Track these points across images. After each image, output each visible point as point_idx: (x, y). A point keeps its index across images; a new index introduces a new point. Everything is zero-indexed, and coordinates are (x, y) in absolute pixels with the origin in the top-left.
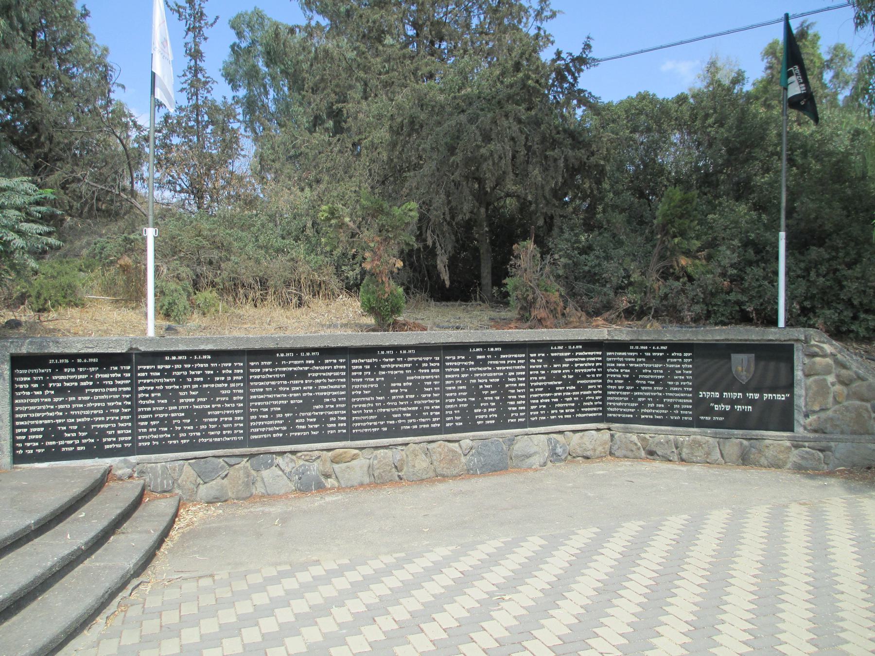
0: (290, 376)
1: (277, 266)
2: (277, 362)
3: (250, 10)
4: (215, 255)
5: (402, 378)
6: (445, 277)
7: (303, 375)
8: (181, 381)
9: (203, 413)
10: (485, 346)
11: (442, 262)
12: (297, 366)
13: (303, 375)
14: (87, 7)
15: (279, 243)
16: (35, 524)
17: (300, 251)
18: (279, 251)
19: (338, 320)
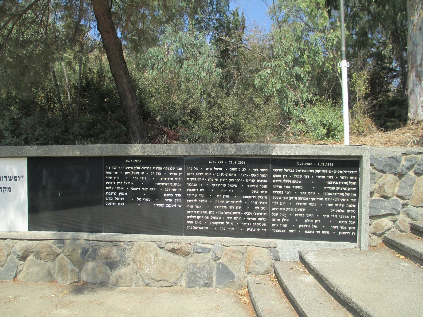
9: (292, 134)
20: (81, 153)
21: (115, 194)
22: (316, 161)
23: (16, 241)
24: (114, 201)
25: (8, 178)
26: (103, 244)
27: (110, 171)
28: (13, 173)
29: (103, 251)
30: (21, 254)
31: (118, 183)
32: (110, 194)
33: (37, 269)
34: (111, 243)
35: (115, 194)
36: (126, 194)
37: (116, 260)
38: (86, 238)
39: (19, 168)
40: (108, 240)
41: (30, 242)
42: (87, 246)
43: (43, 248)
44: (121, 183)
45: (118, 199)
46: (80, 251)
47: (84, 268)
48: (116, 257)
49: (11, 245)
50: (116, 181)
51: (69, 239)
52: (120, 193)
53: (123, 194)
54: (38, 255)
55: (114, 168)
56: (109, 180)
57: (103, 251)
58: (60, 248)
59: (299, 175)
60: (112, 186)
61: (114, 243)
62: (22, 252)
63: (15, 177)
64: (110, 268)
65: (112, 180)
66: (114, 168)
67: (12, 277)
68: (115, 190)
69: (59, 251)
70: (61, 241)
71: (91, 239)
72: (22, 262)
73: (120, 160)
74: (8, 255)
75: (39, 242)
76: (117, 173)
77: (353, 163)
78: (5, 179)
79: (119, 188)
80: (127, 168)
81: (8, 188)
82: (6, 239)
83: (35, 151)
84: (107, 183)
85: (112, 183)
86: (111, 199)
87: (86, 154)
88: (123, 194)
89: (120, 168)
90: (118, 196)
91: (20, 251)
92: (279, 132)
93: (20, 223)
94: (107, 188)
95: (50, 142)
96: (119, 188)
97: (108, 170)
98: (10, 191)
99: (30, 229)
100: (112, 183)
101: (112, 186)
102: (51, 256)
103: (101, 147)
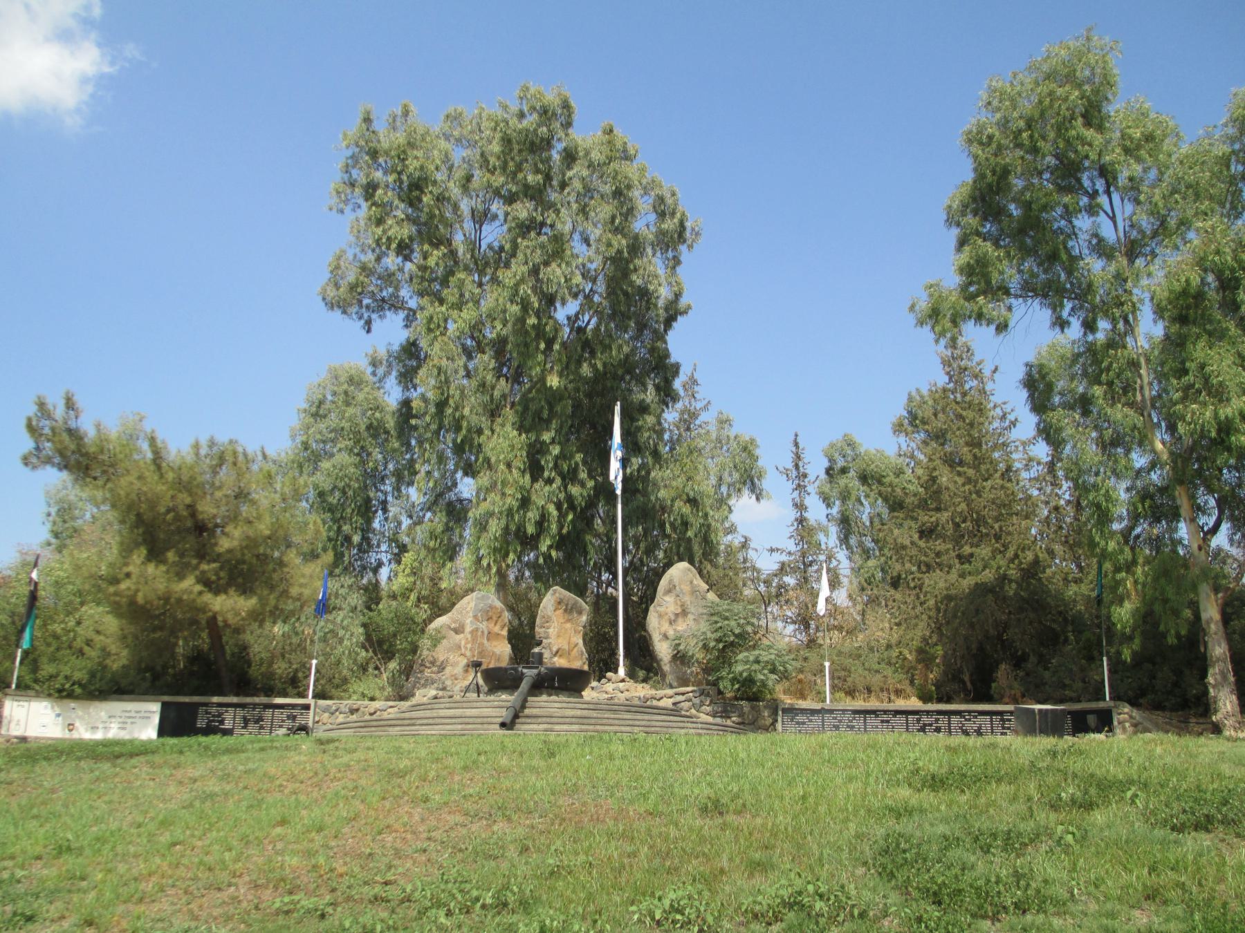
0: (882, 721)
1: (876, 680)
2: (877, 716)
3: (324, 375)
4: (843, 673)
5: (931, 725)
6: (969, 684)
7: (888, 722)
8: (840, 721)
10: (970, 712)
11: (966, 678)
12: (885, 717)
13: (888, 722)
14: (100, 419)
15: (876, 667)
16: (541, 694)
17: (889, 671)
18: (877, 671)
19: (914, 703)
22: (293, 706)
27: (202, 709)
39: (155, 708)
59: (286, 712)
73: (206, 705)
77: (307, 707)
83: (166, 698)
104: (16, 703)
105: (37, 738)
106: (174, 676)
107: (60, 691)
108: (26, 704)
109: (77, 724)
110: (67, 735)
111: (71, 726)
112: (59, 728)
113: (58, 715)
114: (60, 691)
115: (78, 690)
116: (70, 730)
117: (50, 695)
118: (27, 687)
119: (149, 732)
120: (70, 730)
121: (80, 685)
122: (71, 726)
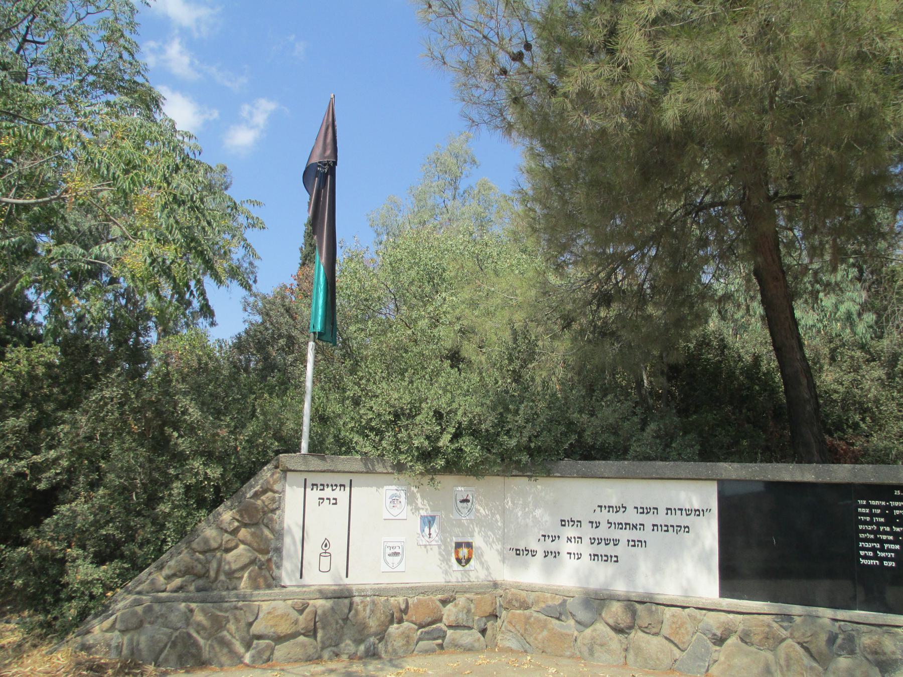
20: (817, 477)
21: (878, 546)
23: (704, 612)
24: (875, 557)
25: (684, 512)
26: (864, 628)
28: (692, 505)
29: (866, 640)
30: (719, 633)
31: (882, 528)
32: (868, 545)
33: (745, 660)
34: (878, 629)
35: (878, 546)
36: (898, 547)
37: (894, 657)
38: (831, 617)
39: (695, 500)
40: (874, 622)
41: (731, 616)
42: (836, 629)
43: (756, 625)
44: (888, 529)
45: (883, 554)
46: (824, 637)
47: (832, 666)
48: (893, 653)
49: (699, 617)
50: (879, 524)
51: (800, 616)
52: (886, 546)
53: (892, 546)
54: (745, 638)
55: (873, 503)
56: (865, 523)
57: (866, 640)
58: (785, 629)
60: (871, 532)
61: (885, 628)
62: (721, 630)
63: (695, 511)
64: (881, 671)
65: (871, 523)
66: (873, 503)
67: (704, 670)
68: (876, 540)
69: (784, 633)
70: (788, 617)
71: (839, 618)
72: (718, 648)
74: (694, 633)
75: (746, 616)
76: (879, 511)
78: (679, 512)
79: (884, 537)
80: (897, 504)
81: (685, 528)
82: (689, 607)
83: (731, 470)
84: (861, 527)
85: (870, 528)
86: (871, 554)
87: (827, 479)
88: (892, 546)
89: (883, 503)
90: (882, 550)
91: (718, 628)
92: (773, 391)
93: (706, 585)
94: (862, 536)
95: (635, 448)
96: (884, 537)
97: (863, 506)
98: (688, 532)
99: (722, 595)
100: (870, 528)
101: (871, 532)
102: (771, 641)
103: (854, 468)
104: (313, 495)
105: (378, 593)
106: (170, 436)
107: (426, 456)
108: (342, 495)
109: (478, 541)
110: (456, 575)
111: (464, 552)
112: (434, 555)
113: (429, 521)
114: (426, 456)
115: (471, 449)
116: (463, 562)
117: (400, 468)
118: (344, 447)
119: (688, 569)
120: (463, 562)
121: (475, 433)
122: (464, 552)
